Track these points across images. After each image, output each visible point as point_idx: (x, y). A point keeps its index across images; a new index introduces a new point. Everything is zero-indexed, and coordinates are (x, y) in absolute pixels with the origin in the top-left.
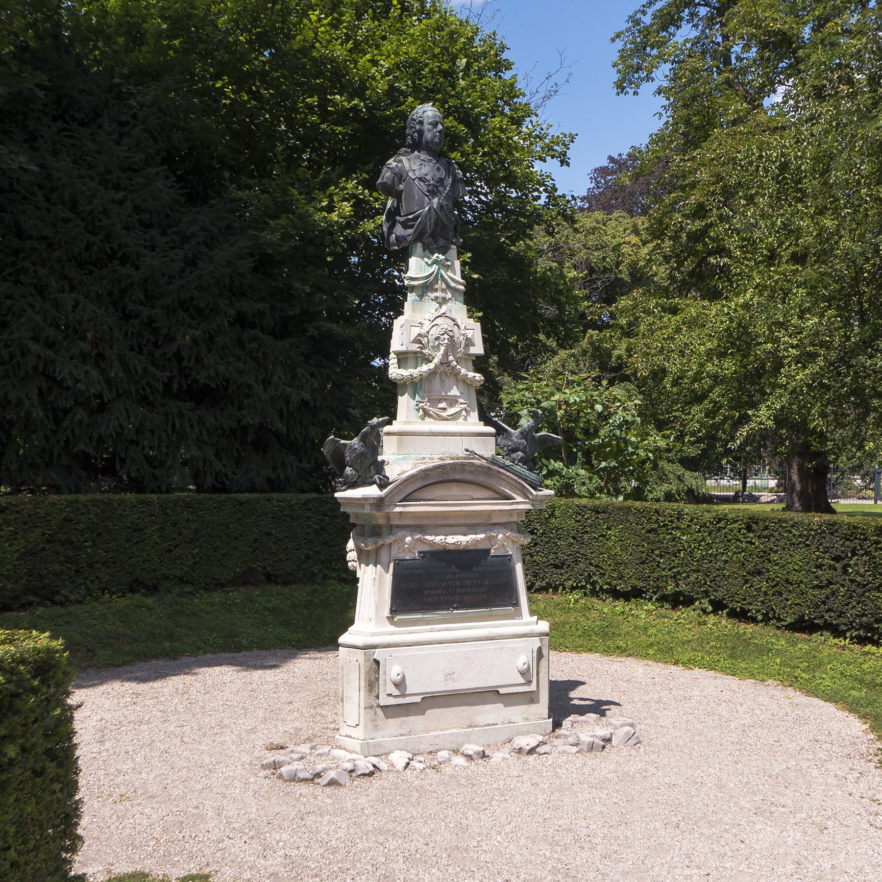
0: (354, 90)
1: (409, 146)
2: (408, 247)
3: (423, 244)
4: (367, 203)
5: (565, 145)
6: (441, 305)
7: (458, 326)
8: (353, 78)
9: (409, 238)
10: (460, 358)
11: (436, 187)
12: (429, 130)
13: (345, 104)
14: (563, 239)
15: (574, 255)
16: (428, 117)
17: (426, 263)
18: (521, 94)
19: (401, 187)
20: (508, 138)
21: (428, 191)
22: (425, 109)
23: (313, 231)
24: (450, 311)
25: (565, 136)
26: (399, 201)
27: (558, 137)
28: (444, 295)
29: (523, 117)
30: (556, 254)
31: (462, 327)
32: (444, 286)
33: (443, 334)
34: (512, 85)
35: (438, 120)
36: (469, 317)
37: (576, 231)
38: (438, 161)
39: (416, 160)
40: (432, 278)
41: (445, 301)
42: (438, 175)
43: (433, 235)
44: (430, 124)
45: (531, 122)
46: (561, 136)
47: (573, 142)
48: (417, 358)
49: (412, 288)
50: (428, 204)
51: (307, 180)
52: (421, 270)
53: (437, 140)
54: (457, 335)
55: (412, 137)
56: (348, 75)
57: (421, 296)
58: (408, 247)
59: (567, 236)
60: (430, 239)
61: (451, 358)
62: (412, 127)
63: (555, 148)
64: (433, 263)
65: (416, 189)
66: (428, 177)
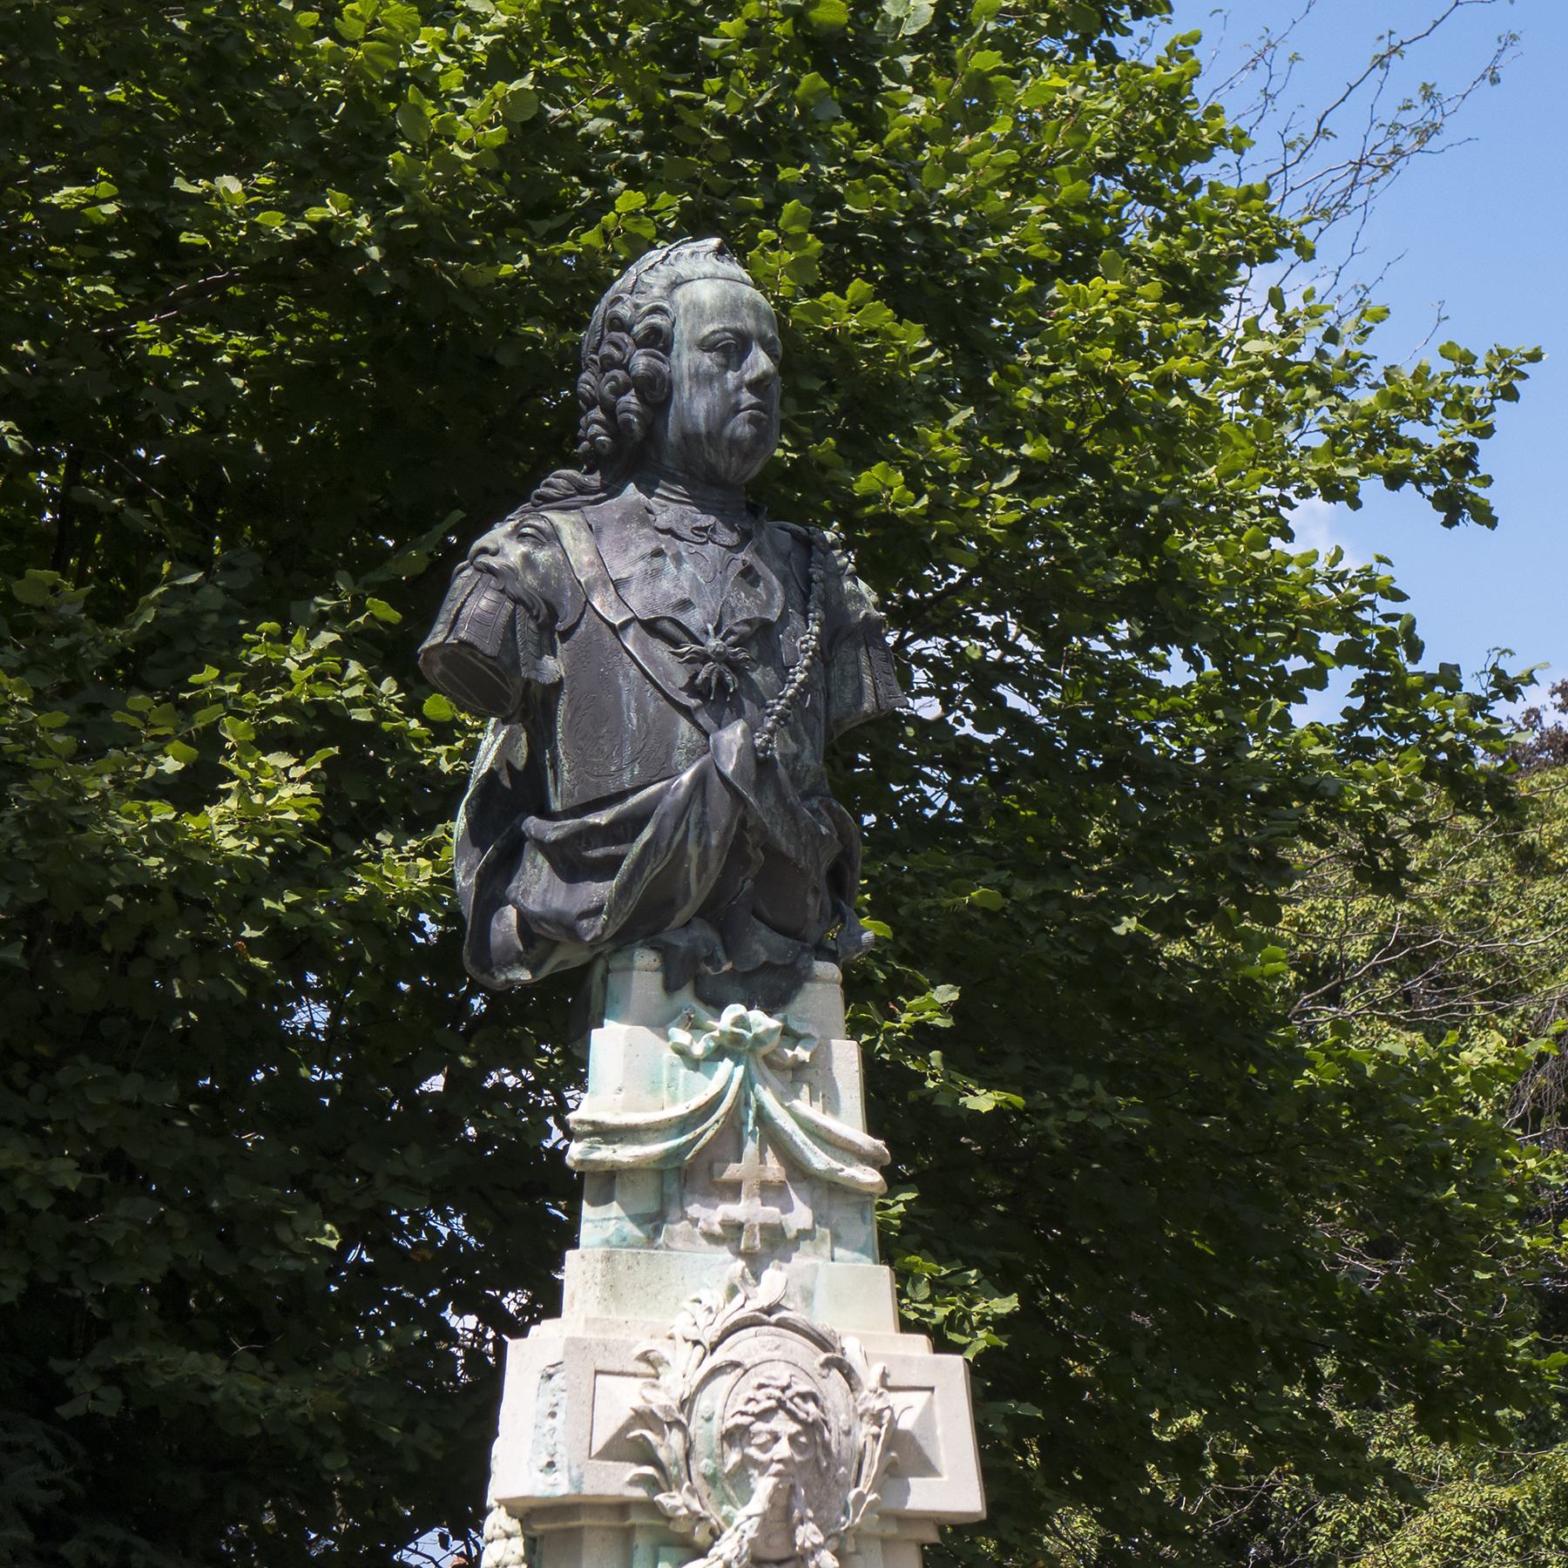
0: (315, 146)
1: (593, 461)
2: (587, 968)
3: (666, 953)
4: (395, 743)
5: (1470, 414)
6: (755, 1263)
7: (848, 1373)
8: (315, 84)
9: (591, 929)
10: (857, 1533)
11: (736, 666)
12: (703, 379)
13: (274, 221)
14: (1459, 903)
15: (1522, 990)
16: (697, 308)
17: (682, 1052)
18: (1221, 138)
19: (553, 667)
20: (1165, 384)
21: (692, 689)
22: (683, 268)
23: (96, 897)
24: (808, 1296)
25: (1466, 364)
26: (541, 736)
27: (1420, 375)
28: (772, 1213)
29: (1233, 261)
30: (1417, 983)
31: (869, 1377)
32: (774, 1169)
33: (764, 1415)
34: (1175, 94)
35: (749, 323)
36: (906, 1326)
37: (1531, 862)
38: (746, 537)
39: (632, 530)
40: (710, 1128)
41: (777, 1243)
42: (746, 606)
43: (714, 911)
44: (706, 345)
45: (1276, 298)
46: (1439, 366)
47: (1511, 394)
48: (628, 1534)
49: (609, 1181)
50: (692, 755)
51: (66, 629)
52: (654, 1087)
53: (741, 427)
54: (839, 1419)
55: (610, 410)
56: (284, 65)
57: (653, 1222)
58: (587, 968)
59: (1482, 893)
60: (704, 933)
61: (807, 1534)
62: (608, 364)
63: (1409, 430)
64: (719, 1053)
65: (628, 681)
66: (694, 619)
